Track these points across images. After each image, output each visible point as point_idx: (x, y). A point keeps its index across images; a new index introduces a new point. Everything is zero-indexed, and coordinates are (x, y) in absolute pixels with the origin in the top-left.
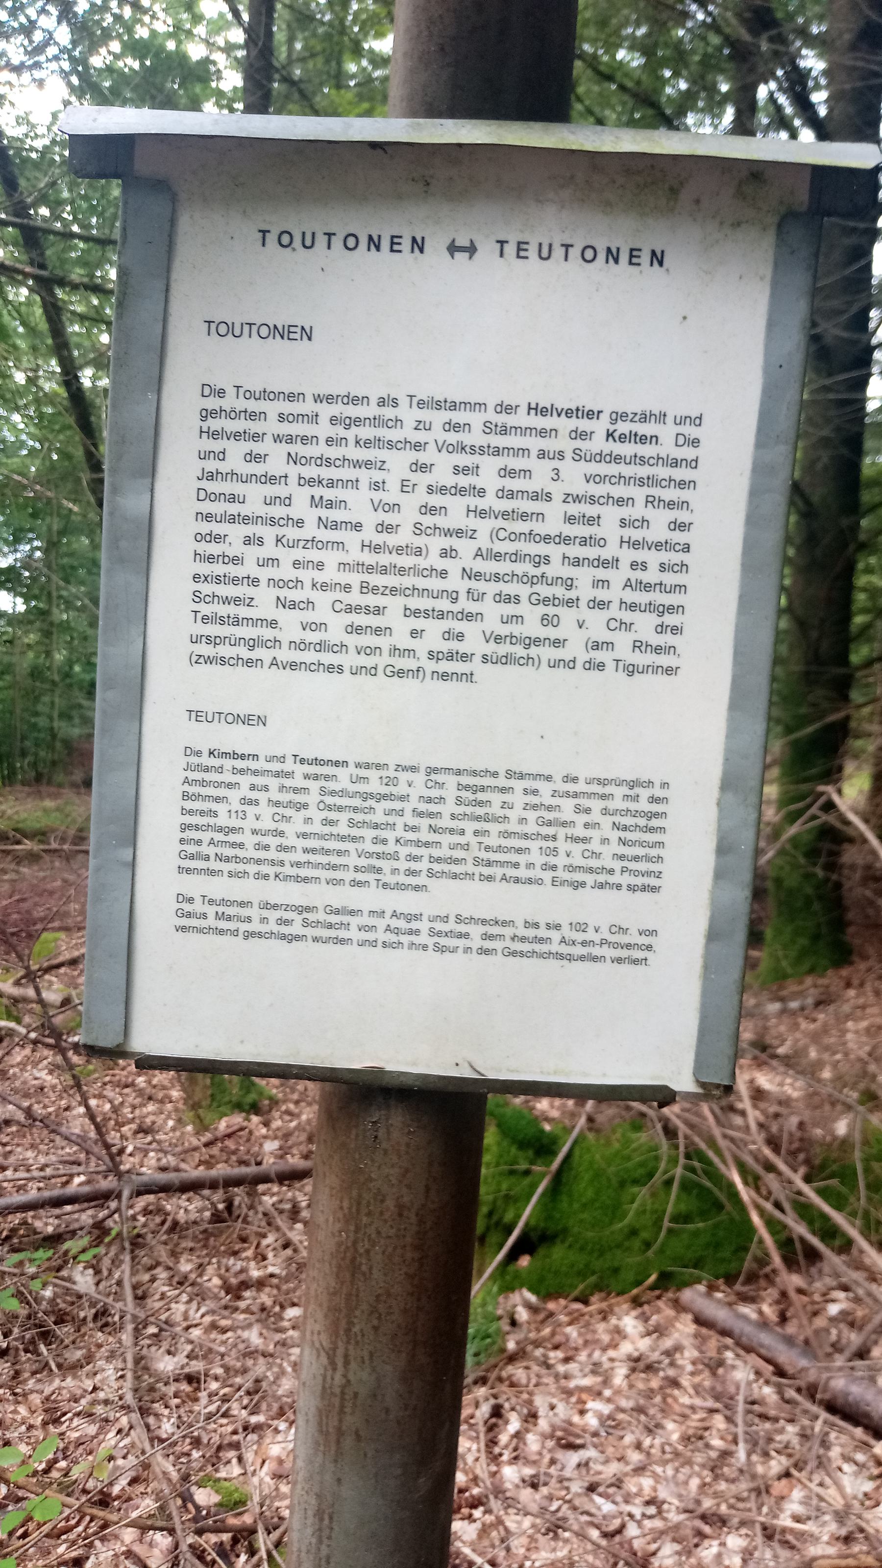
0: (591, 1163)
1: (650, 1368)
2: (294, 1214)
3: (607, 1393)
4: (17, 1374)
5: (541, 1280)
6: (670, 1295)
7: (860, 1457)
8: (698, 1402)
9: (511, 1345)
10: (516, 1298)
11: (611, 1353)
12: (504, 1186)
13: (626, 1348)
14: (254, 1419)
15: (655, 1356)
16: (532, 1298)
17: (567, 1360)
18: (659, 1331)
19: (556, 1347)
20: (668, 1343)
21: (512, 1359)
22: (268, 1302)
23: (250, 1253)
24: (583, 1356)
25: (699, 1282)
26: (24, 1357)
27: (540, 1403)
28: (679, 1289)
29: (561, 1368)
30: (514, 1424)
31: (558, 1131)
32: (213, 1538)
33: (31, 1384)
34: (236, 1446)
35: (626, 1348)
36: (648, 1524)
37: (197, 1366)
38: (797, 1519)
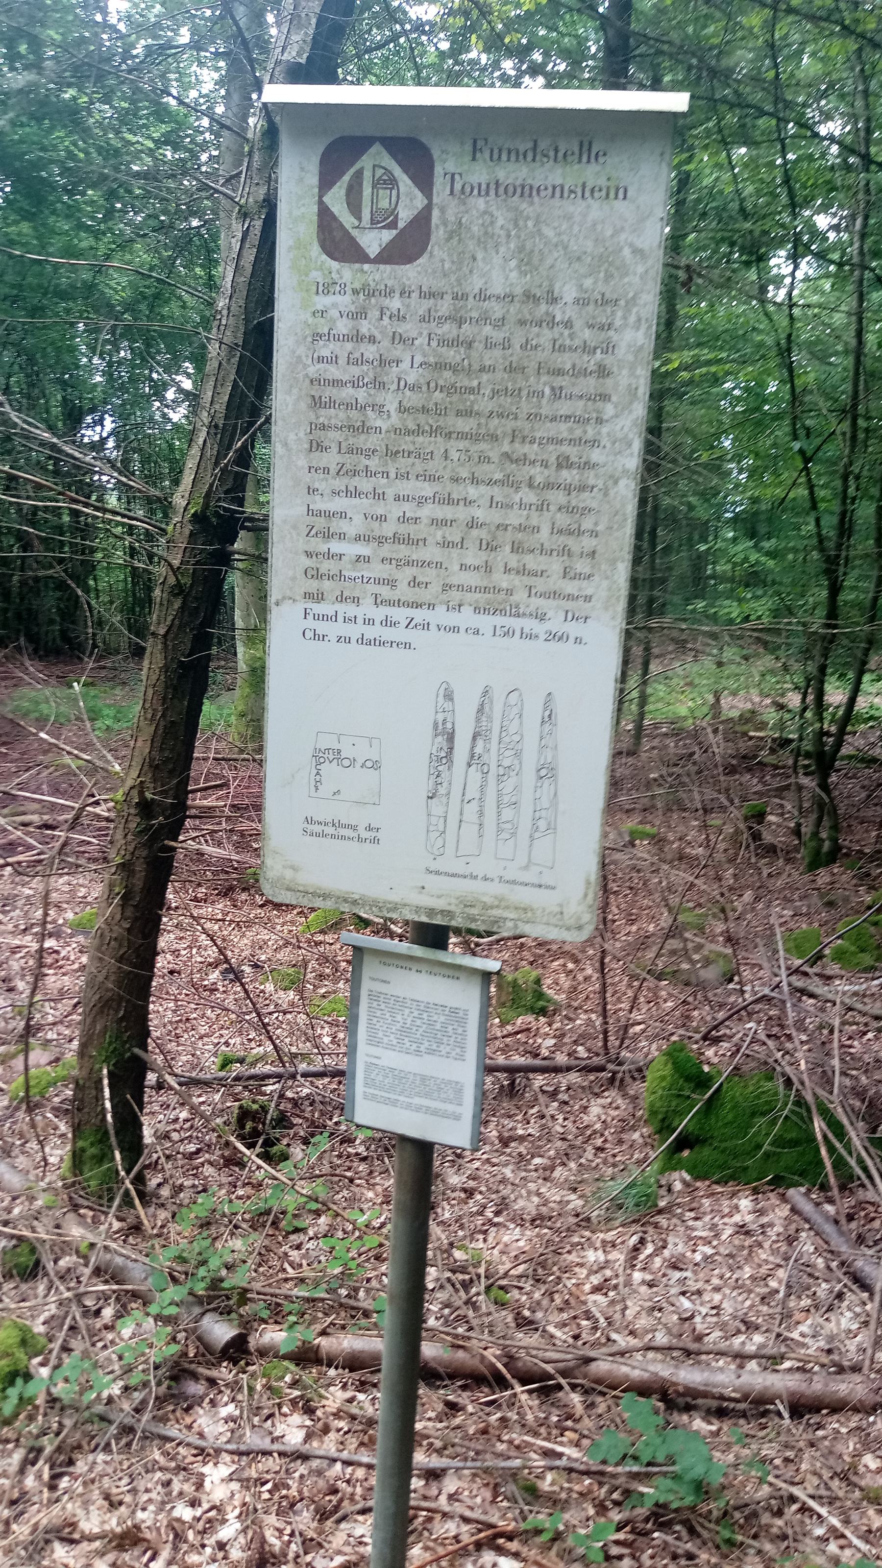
0: (733, 1098)
1: (747, 1233)
2: (554, 1095)
3: (715, 1243)
4: (371, 1172)
5: (695, 1167)
6: (781, 1191)
7: (858, 1310)
8: (771, 1259)
9: (662, 1204)
10: (676, 1175)
11: (726, 1220)
12: (674, 1104)
13: (737, 1218)
14: (496, 1220)
15: (753, 1227)
16: (688, 1177)
17: (696, 1219)
18: (761, 1212)
19: (691, 1210)
20: (765, 1220)
21: (660, 1212)
22: (525, 1152)
23: (519, 1117)
24: (707, 1219)
25: (802, 1185)
26: (377, 1163)
27: (671, 1240)
28: (788, 1188)
29: (691, 1223)
30: (649, 1249)
31: (713, 1073)
32: (461, 1277)
33: (378, 1180)
34: (485, 1232)
35: (737, 1218)
36: (709, 1319)
37: (472, 1184)
38: (803, 1335)
